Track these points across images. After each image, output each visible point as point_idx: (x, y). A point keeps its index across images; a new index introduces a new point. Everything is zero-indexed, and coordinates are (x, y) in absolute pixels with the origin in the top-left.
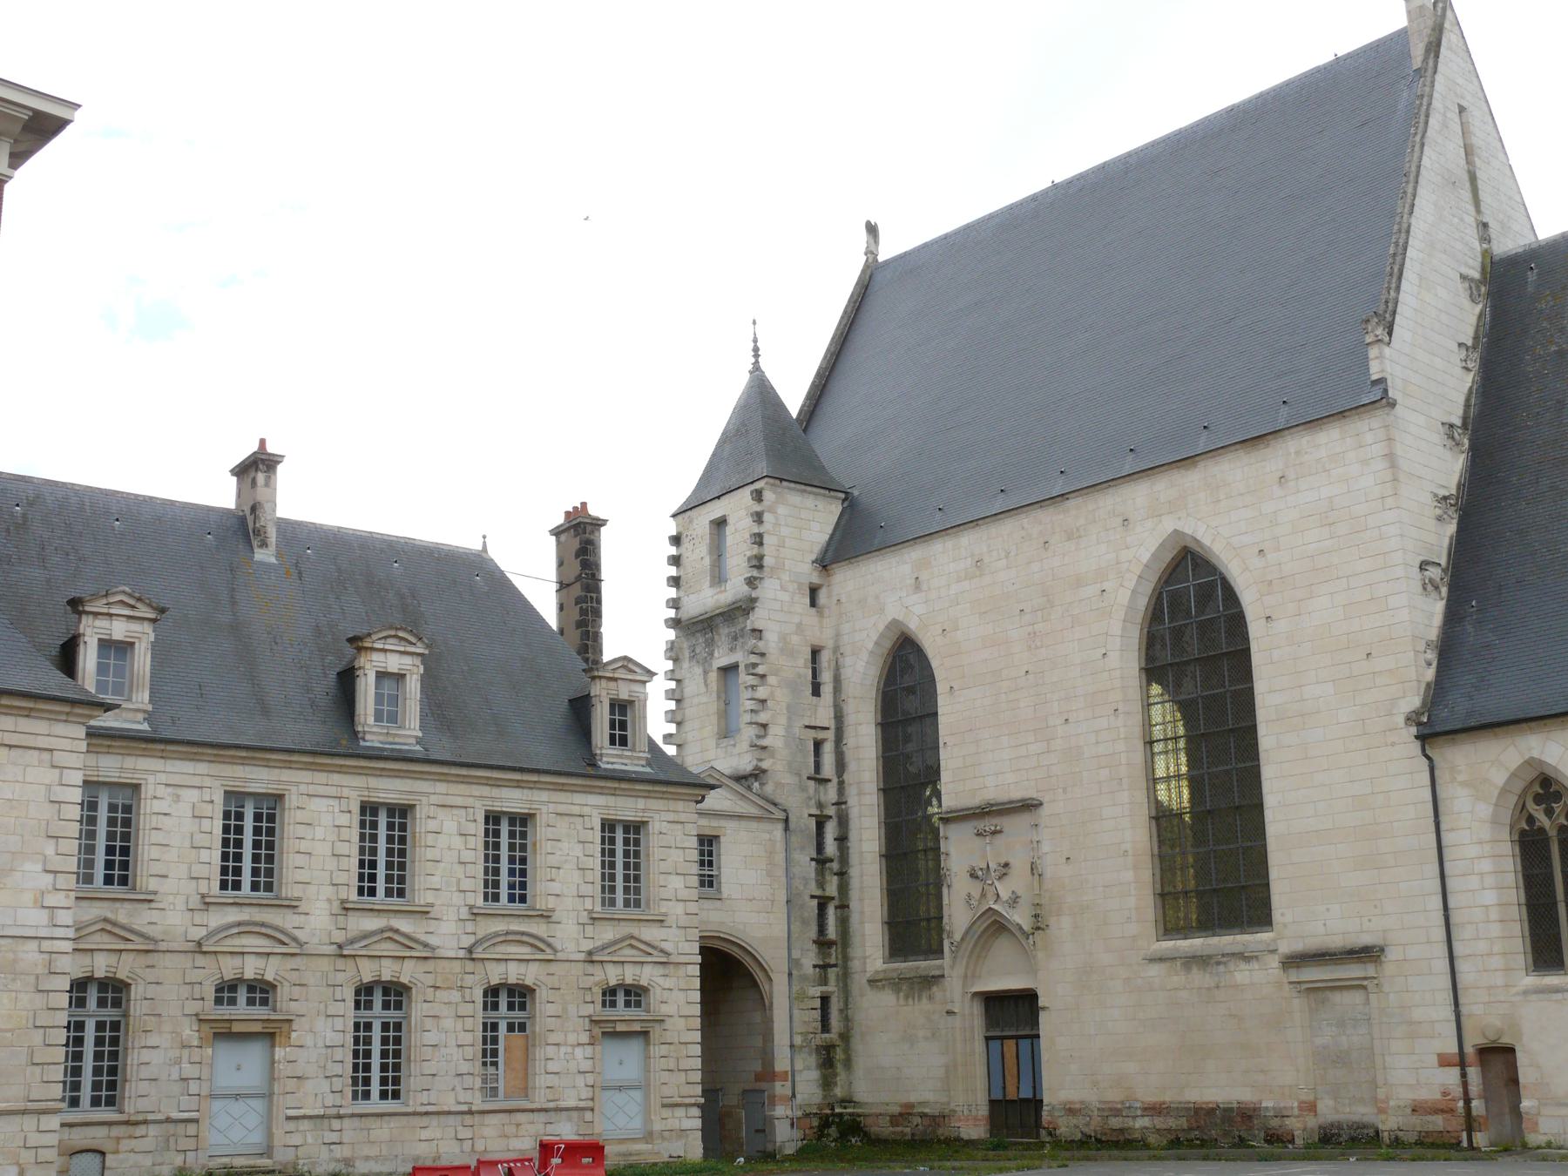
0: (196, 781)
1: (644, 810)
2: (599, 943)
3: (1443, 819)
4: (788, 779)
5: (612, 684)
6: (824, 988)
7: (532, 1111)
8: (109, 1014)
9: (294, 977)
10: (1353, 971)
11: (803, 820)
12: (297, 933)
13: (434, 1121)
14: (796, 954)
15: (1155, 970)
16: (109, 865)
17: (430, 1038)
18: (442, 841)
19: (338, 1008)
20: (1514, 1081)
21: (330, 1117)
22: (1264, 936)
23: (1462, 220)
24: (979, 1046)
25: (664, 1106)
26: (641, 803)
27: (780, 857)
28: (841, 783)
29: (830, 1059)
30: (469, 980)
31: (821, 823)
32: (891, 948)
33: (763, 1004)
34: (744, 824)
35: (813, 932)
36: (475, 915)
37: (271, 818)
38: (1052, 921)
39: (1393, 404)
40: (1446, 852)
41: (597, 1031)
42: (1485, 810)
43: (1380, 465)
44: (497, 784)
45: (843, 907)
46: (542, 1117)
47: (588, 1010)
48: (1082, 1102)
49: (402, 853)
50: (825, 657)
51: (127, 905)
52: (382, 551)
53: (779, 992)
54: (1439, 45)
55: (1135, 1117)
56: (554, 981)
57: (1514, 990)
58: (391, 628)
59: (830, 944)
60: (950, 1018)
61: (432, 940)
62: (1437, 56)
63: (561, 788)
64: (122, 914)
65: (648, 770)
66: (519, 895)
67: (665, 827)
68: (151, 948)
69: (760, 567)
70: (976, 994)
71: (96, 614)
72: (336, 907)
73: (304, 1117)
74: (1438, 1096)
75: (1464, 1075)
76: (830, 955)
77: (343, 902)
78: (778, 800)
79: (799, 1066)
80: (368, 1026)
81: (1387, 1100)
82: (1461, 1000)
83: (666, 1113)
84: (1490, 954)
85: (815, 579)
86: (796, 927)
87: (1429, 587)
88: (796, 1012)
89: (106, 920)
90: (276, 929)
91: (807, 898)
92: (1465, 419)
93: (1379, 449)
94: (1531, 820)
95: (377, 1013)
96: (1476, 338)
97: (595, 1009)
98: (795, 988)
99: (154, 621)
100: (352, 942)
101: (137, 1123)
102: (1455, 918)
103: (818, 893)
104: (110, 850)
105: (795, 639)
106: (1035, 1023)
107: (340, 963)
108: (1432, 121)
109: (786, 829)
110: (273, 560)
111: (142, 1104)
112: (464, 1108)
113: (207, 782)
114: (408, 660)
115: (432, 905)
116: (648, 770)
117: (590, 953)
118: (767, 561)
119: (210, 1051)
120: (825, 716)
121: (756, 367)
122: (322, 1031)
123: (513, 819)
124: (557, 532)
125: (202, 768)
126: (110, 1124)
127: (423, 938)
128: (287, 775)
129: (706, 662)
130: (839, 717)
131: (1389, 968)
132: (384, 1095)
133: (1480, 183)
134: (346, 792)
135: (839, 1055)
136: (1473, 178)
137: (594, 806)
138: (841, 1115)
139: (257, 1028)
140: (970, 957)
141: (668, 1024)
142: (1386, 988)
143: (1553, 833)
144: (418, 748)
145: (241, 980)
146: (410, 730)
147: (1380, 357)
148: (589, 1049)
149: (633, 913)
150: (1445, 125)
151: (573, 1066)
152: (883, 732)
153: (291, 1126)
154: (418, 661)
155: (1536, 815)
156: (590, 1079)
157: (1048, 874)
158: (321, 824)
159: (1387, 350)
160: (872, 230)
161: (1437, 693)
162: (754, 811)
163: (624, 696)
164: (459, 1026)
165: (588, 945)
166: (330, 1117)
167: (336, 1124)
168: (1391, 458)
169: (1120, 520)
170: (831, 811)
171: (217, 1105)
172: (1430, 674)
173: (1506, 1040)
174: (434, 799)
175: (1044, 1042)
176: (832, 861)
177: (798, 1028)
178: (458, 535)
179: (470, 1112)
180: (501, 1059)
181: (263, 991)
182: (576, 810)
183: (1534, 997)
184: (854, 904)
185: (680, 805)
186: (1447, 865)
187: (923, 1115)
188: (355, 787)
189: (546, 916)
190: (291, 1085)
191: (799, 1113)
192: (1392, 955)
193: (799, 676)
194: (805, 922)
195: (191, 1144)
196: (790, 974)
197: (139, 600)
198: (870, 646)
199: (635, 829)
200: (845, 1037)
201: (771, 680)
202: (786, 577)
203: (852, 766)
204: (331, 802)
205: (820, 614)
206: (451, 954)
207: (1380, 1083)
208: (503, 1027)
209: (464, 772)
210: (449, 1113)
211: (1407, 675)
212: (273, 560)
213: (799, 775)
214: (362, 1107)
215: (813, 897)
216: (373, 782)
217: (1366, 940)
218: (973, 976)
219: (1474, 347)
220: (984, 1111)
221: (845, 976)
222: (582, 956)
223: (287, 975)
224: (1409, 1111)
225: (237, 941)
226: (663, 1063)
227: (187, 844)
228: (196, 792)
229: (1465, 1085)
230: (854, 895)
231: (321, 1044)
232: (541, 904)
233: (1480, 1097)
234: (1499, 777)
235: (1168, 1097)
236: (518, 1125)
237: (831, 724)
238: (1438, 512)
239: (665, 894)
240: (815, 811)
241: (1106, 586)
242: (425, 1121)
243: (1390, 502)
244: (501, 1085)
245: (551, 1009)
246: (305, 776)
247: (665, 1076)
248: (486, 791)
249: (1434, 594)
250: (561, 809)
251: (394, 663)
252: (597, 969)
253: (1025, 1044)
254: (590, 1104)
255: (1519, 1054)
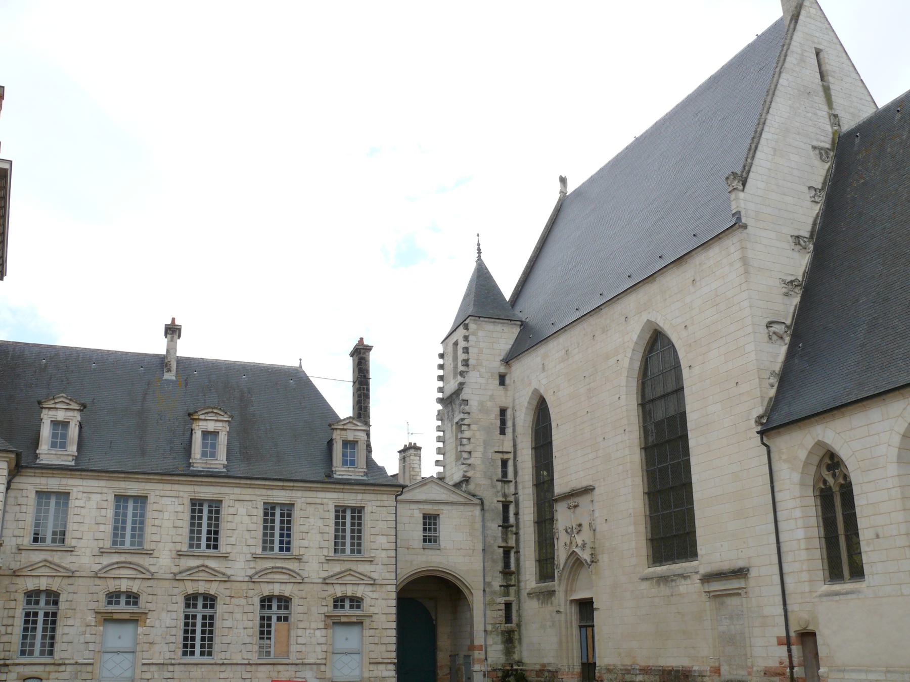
0: (99, 490)
1: (361, 500)
2: (331, 574)
3: (776, 484)
4: (484, 482)
5: (343, 432)
6: (507, 598)
7: (288, 664)
8: (51, 608)
9: (149, 590)
10: (734, 584)
11: (493, 501)
12: (301, 572)
13: (229, 668)
14: (488, 579)
15: (645, 585)
16: (208, 539)
17: (228, 624)
18: (237, 519)
19: (175, 607)
20: (816, 654)
21: (167, 664)
22: (695, 563)
23: (815, 114)
24: (575, 631)
25: (370, 663)
26: (360, 497)
27: (478, 526)
28: (516, 482)
29: (510, 639)
30: (251, 593)
31: (506, 507)
32: (540, 575)
33: (470, 609)
34: (455, 507)
35: (500, 566)
36: (255, 558)
37: (289, 515)
38: (600, 557)
39: (745, 227)
40: (778, 505)
41: (330, 622)
42: (796, 477)
43: (738, 264)
44: (271, 488)
45: (517, 552)
46: (294, 668)
47: (325, 610)
48: (614, 665)
49: (289, 529)
50: (509, 413)
51: (59, 553)
52: (238, 370)
53: (477, 601)
54: (798, 15)
55: (636, 675)
56: (303, 594)
57: (815, 594)
58: (209, 408)
59: (512, 573)
60: (558, 615)
61: (229, 572)
62: (796, 22)
63: (310, 489)
64: (56, 558)
65: (365, 478)
66: (286, 546)
67: (374, 509)
68: (71, 575)
69: (467, 365)
70: (572, 601)
71: (50, 408)
72: (174, 554)
73: (153, 664)
74: (778, 665)
75: (789, 651)
76: (511, 580)
77: (178, 551)
78: (477, 493)
79: (490, 641)
80: (194, 617)
81: (752, 666)
82: (788, 602)
83: (372, 667)
84: (802, 571)
85: (503, 370)
86: (488, 564)
87: (774, 337)
88: (488, 612)
89: (45, 561)
90: (138, 565)
91: (496, 548)
92: (812, 233)
93: (737, 255)
94: (825, 482)
95: (200, 610)
96: (824, 183)
97: (329, 609)
98: (487, 599)
99: (80, 410)
100: (180, 573)
101: (60, 665)
102: (783, 549)
103: (504, 544)
104: (209, 532)
105: (489, 404)
106: (592, 619)
107: (176, 584)
108: (789, 59)
109: (483, 509)
110: (174, 378)
111: (64, 655)
112: (246, 662)
113: (105, 490)
114: (220, 424)
115: (229, 553)
116: (365, 478)
117: (324, 579)
118: (471, 362)
119: (101, 628)
120: (508, 446)
121: (479, 260)
122: (166, 619)
123: (353, 509)
124: (352, 355)
125: (102, 483)
126: (45, 664)
127: (223, 570)
128: (149, 486)
129: (451, 420)
130: (515, 446)
131: (752, 582)
132: (202, 654)
133: (833, 93)
134: (181, 494)
135: (516, 636)
136: (827, 90)
137: (330, 499)
138: (516, 670)
139: (127, 617)
140: (568, 579)
141: (375, 618)
142: (751, 595)
143: (836, 489)
144: (224, 470)
145: (346, 597)
146: (221, 459)
147: (737, 199)
148: (324, 631)
149: (356, 556)
150: (802, 60)
151: (314, 640)
152: (536, 452)
153: (145, 668)
154: (226, 425)
155: (827, 478)
156: (324, 648)
157: (599, 529)
158: (168, 510)
159: (741, 195)
160: (563, 180)
161: (775, 405)
162: (462, 500)
163: (351, 438)
164: (245, 618)
165: (324, 575)
166: (167, 664)
167: (171, 668)
168: (745, 261)
169: (624, 318)
170: (512, 499)
171: (107, 656)
172: (772, 392)
173: (811, 628)
174: (232, 497)
175: (595, 628)
176: (512, 526)
177: (489, 620)
178: (290, 361)
179: (249, 664)
180: (272, 636)
181: (357, 602)
182: (318, 501)
183: (824, 599)
184: (521, 551)
185: (385, 497)
186: (779, 514)
187: (549, 671)
188: (186, 492)
189: (299, 559)
190: (146, 647)
191: (489, 669)
192: (753, 573)
193: (492, 424)
194: (494, 561)
195: (89, 676)
196: (484, 591)
197: (71, 400)
198: (526, 404)
199: (358, 512)
200: (519, 625)
201: (473, 427)
202: (483, 370)
203: (520, 473)
204: (173, 499)
205: (506, 390)
206: (241, 579)
207: (749, 656)
208: (274, 618)
209: (248, 482)
210: (237, 664)
211: (755, 396)
212: (174, 378)
213: (491, 479)
214: (189, 659)
215: (499, 547)
216: (197, 489)
217: (740, 564)
218: (571, 590)
219: (823, 189)
220: (578, 669)
221: (518, 592)
222: (320, 581)
223: (145, 589)
224: (762, 674)
225: (117, 572)
226: (371, 640)
227: (93, 522)
228: (99, 496)
229: (790, 657)
230: (522, 545)
231: (163, 626)
232: (147, 546)
233: (800, 665)
234: (803, 455)
235: (651, 663)
236: (279, 672)
237: (511, 449)
238: (784, 290)
239: (374, 546)
240: (501, 499)
241: (619, 357)
242: (223, 668)
243: (744, 287)
244: (272, 650)
245: (300, 609)
246: (372, 497)
247: (372, 647)
248: (264, 492)
249: (779, 342)
250: (309, 500)
251: (211, 426)
252: (330, 588)
253: (590, 629)
254: (324, 661)
255: (818, 637)
